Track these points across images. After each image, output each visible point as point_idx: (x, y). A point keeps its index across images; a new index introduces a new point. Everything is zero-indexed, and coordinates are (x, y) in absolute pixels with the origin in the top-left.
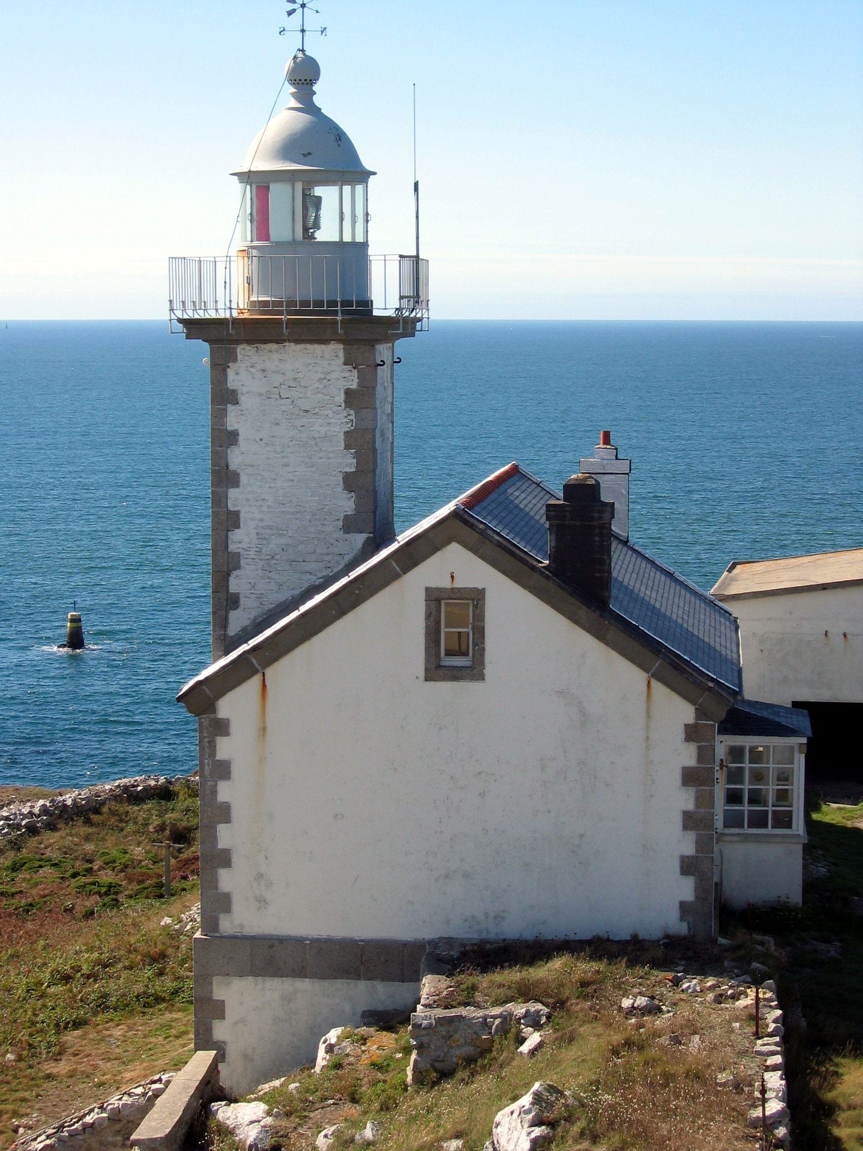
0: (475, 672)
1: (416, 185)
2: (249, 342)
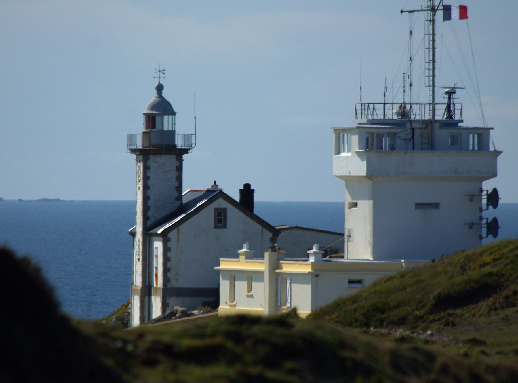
0: (225, 226)
1: (195, 118)
2: (153, 155)
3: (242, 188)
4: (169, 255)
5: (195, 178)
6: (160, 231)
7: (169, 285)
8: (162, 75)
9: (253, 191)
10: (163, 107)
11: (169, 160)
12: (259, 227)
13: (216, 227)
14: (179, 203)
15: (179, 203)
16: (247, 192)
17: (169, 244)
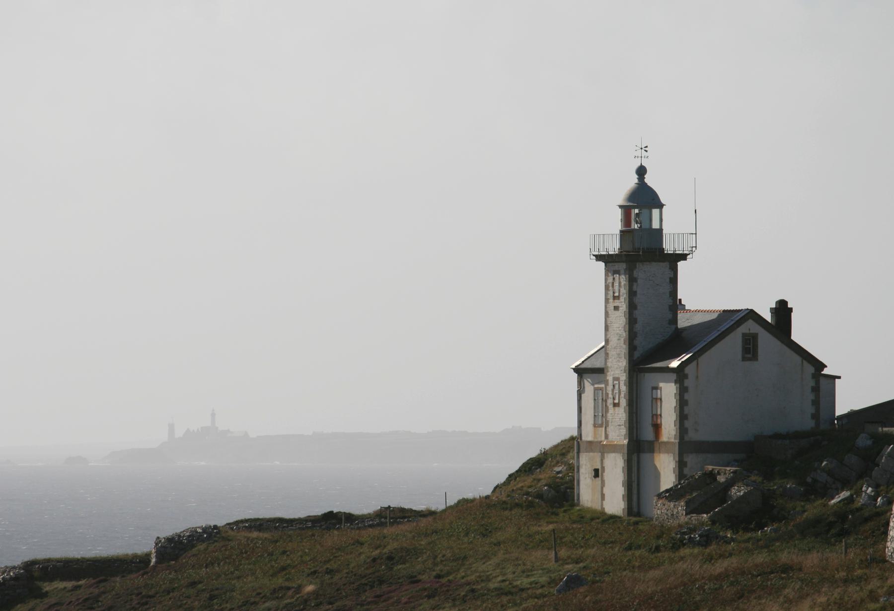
2: (641, 261)
3: (774, 306)
4: (686, 397)
5: (702, 292)
6: (675, 364)
7: (686, 438)
8: (644, 153)
9: (791, 310)
10: (643, 199)
11: (659, 269)
12: (797, 358)
13: (744, 359)
14: (673, 327)
15: (673, 327)
16: (783, 311)
17: (687, 383)
